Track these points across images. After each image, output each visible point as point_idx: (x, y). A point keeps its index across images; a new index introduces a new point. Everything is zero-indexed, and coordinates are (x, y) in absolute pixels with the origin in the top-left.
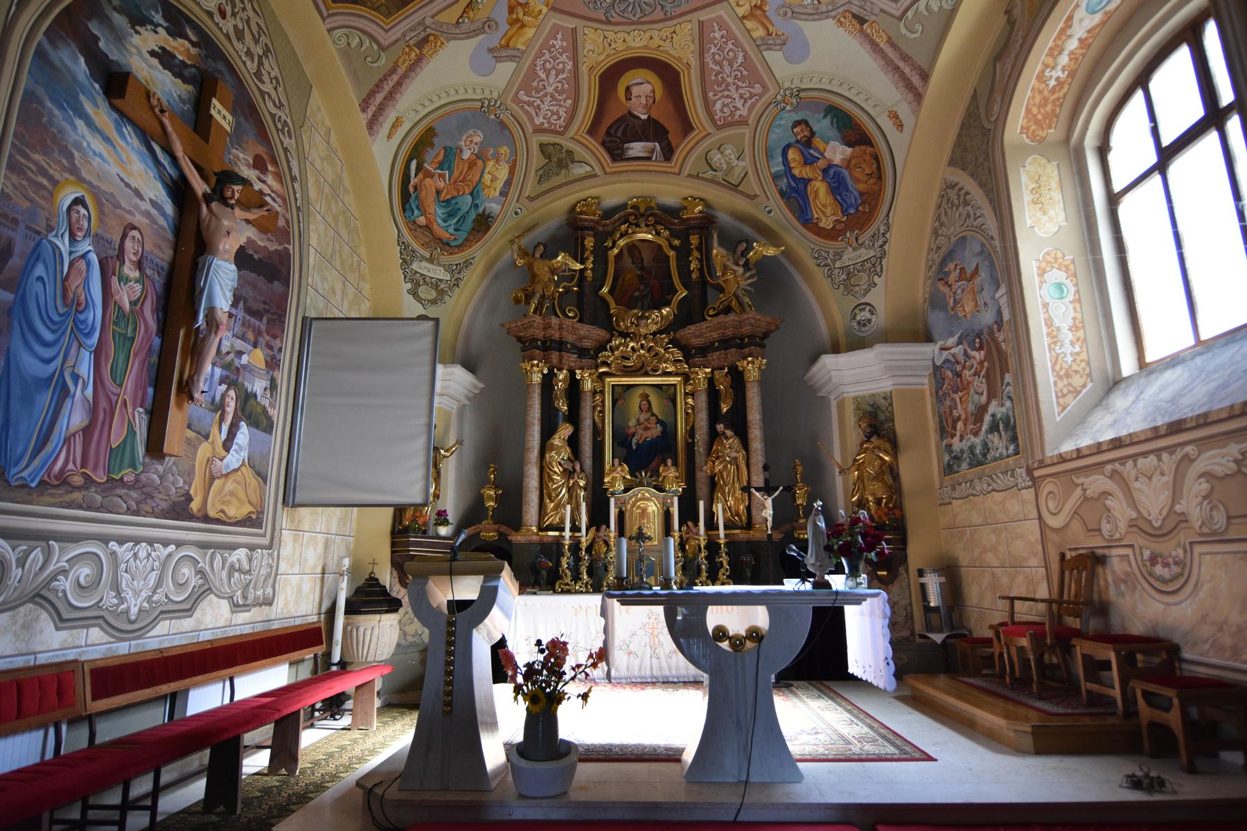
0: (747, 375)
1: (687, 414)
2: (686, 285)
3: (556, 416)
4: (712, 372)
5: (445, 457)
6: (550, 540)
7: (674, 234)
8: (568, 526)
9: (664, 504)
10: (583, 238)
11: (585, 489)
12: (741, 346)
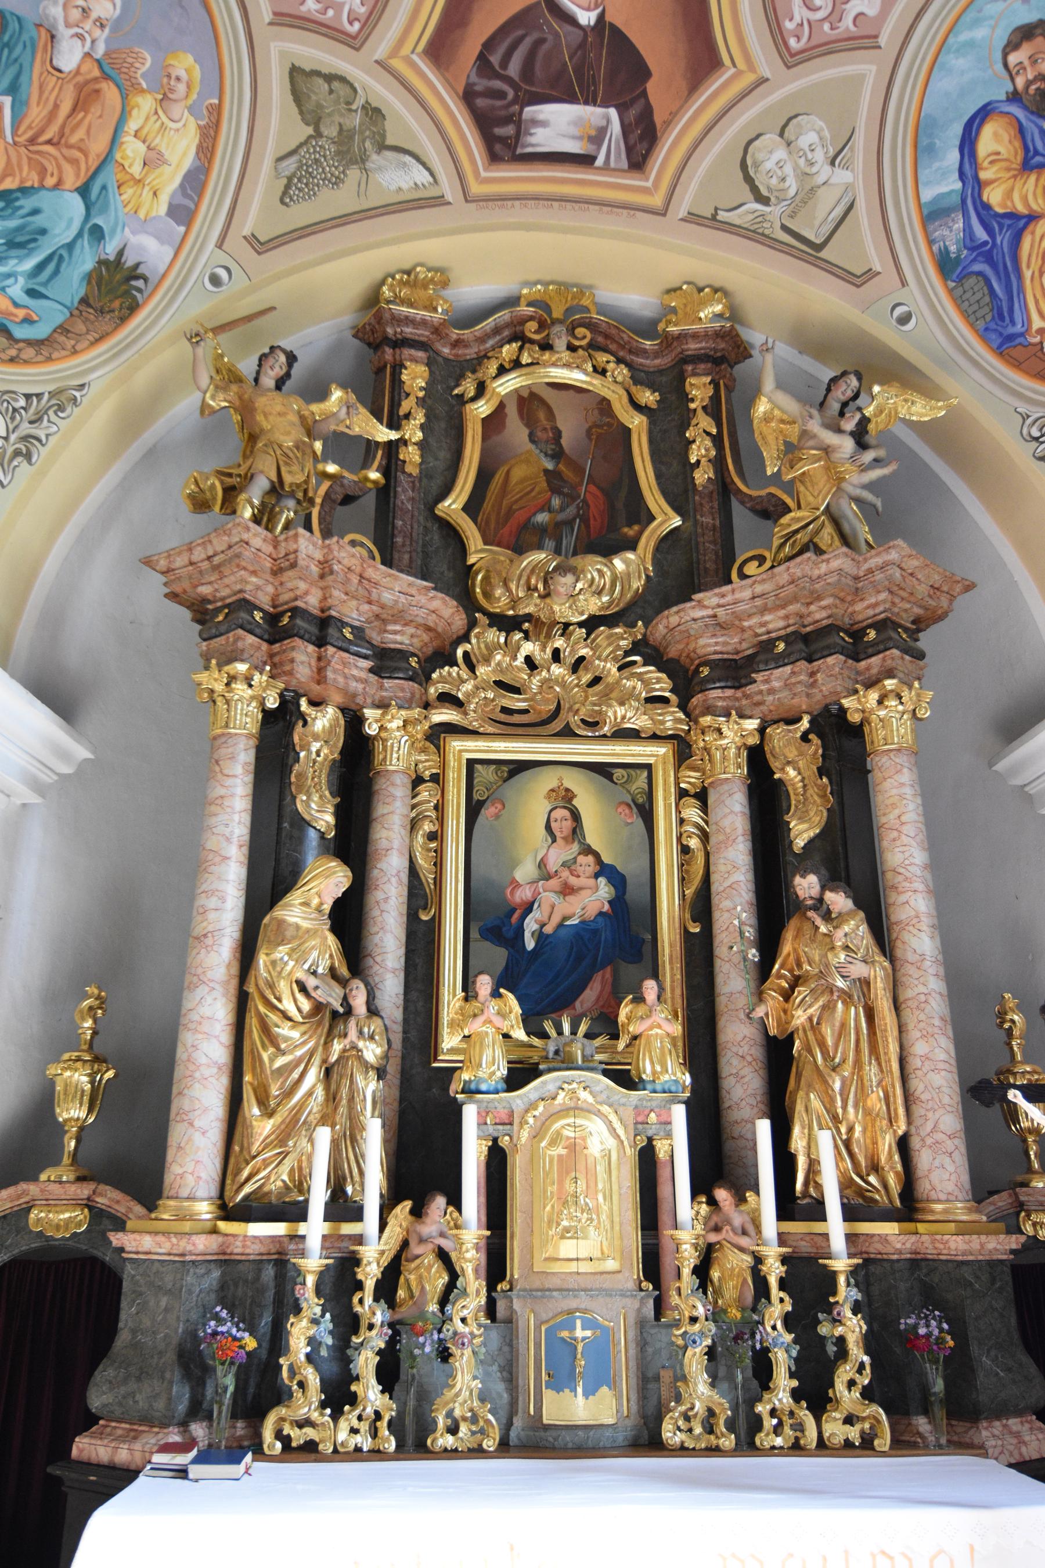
0: (876, 735)
1: (685, 850)
2: (679, 495)
3: (300, 840)
4: (762, 730)
6: (254, 1250)
7: (640, 377)
8: (319, 1197)
9: (639, 1125)
10: (398, 367)
11: (381, 1073)
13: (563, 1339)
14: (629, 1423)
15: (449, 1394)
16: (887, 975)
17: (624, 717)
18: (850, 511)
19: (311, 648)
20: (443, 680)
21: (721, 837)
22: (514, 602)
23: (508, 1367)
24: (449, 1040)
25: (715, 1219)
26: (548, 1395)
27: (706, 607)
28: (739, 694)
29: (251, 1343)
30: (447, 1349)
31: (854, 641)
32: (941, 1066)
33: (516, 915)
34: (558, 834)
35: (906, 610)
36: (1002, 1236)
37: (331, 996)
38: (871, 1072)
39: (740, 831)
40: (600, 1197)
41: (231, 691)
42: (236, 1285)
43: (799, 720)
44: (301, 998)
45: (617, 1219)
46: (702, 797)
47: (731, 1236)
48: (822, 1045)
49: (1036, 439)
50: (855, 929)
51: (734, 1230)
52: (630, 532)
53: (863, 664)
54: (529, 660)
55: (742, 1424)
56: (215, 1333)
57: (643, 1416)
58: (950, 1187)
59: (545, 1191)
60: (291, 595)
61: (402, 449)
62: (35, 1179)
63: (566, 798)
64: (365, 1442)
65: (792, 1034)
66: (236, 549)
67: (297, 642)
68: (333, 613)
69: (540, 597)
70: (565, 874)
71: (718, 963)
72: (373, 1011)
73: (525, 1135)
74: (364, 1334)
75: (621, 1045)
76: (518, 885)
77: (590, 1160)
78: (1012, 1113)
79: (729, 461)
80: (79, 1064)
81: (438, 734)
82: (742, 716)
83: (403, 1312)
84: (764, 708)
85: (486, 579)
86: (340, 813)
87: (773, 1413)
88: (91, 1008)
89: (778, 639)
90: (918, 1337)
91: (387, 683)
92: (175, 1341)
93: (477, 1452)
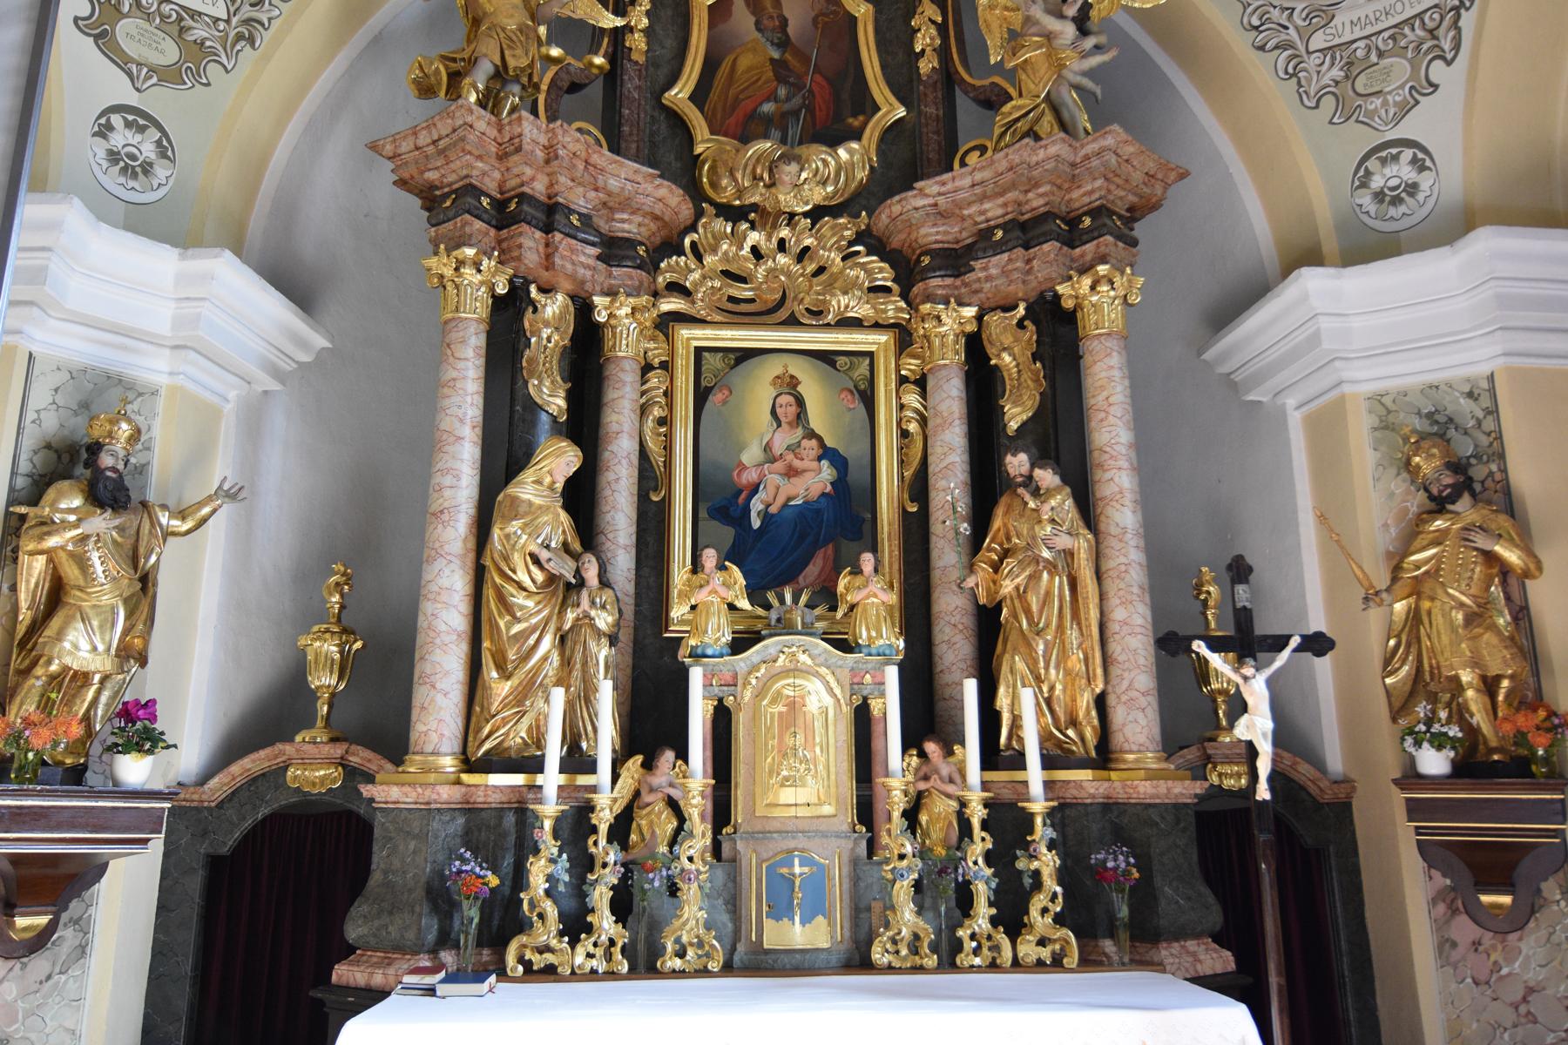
1: (905, 434)
2: (904, 84)
3: (532, 423)
4: (979, 318)
5: (168, 534)
6: (495, 799)
8: (554, 752)
9: (855, 686)
11: (613, 640)
12: (1072, 236)
13: (782, 875)
14: (842, 947)
15: (677, 923)
16: (1090, 547)
17: (847, 307)
18: (1071, 98)
19: (538, 234)
20: (670, 269)
21: (939, 421)
22: (740, 192)
23: (732, 900)
24: (678, 611)
25: (925, 769)
26: (768, 924)
27: (927, 196)
28: (958, 282)
29: (494, 881)
30: (675, 884)
31: (1069, 228)
32: (1139, 630)
33: (743, 496)
34: (783, 419)
35: (1121, 198)
36: (1187, 782)
37: (565, 568)
38: (1072, 635)
39: (957, 415)
40: (818, 750)
41: (460, 276)
42: (480, 830)
43: (1015, 307)
44: (534, 569)
45: (832, 769)
46: (921, 383)
47: (939, 784)
48: (1028, 612)
49: (1256, 28)
50: (1062, 503)
51: (941, 779)
52: (855, 122)
53: (1078, 250)
54: (755, 250)
55: (944, 945)
56: (460, 872)
57: (855, 941)
58: (1142, 739)
59: (766, 744)
60: (518, 181)
61: (628, 36)
62: (291, 740)
63: (793, 383)
64: (602, 967)
65: (1000, 603)
66: (460, 133)
67: (525, 227)
68: (561, 200)
69: (765, 186)
70: (790, 457)
71: (933, 539)
72: (604, 583)
73: (748, 694)
74: (598, 871)
75: (840, 614)
76: (745, 468)
77: (809, 717)
78: (1202, 672)
79: (954, 50)
80: (328, 636)
81: (666, 323)
82: (961, 304)
83: (635, 854)
84: (982, 296)
85: (713, 169)
86: (570, 397)
87: (973, 937)
88: (337, 584)
89: (997, 227)
90: (1106, 869)
91: (616, 271)
92: (424, 879)
93: (704, 972)
